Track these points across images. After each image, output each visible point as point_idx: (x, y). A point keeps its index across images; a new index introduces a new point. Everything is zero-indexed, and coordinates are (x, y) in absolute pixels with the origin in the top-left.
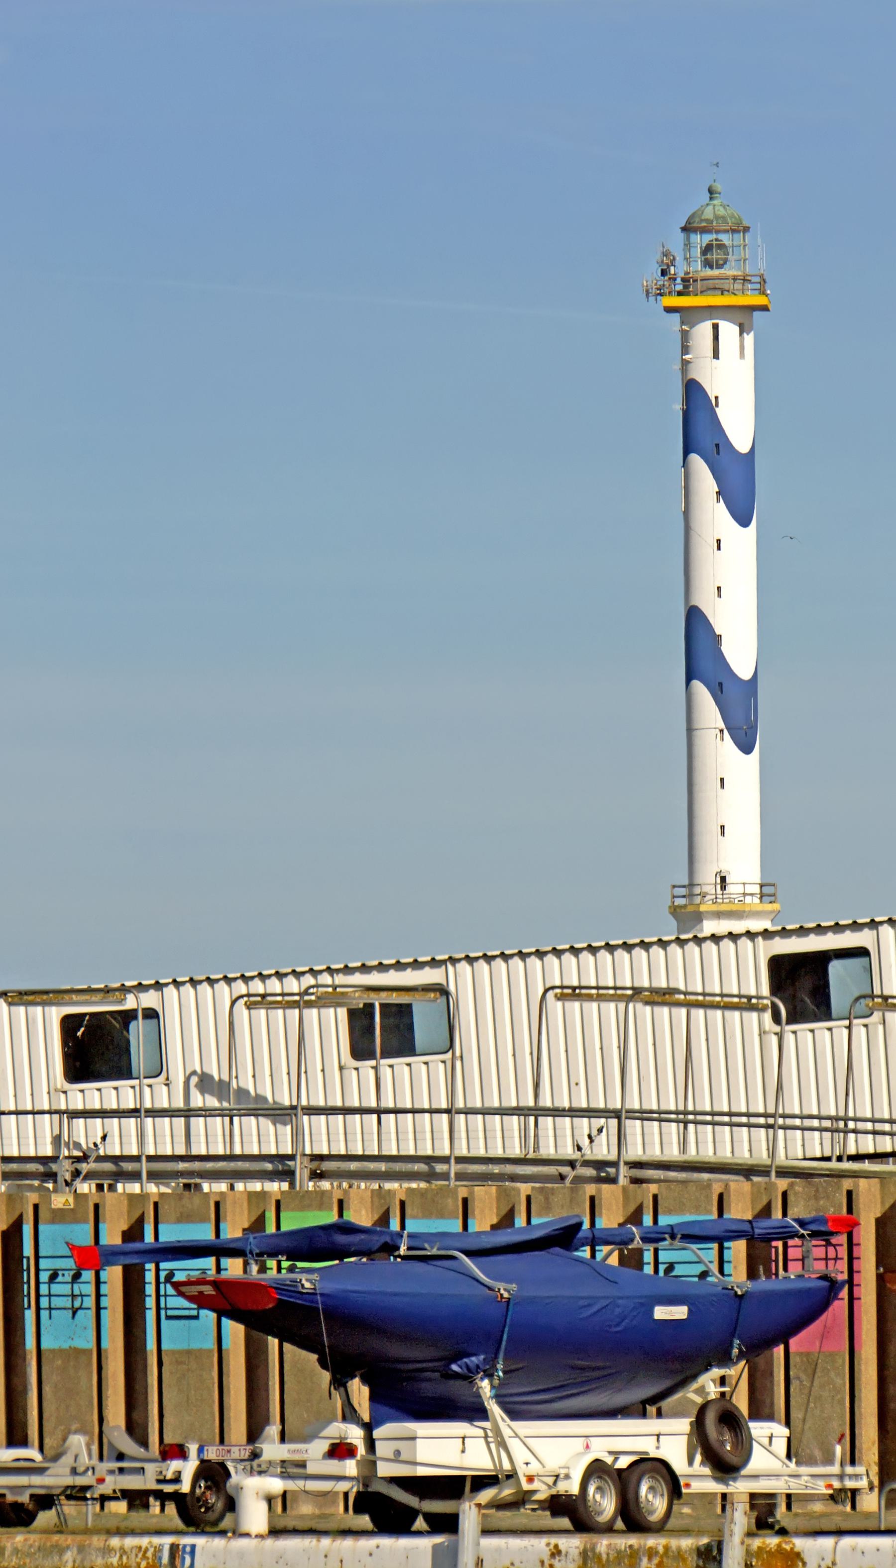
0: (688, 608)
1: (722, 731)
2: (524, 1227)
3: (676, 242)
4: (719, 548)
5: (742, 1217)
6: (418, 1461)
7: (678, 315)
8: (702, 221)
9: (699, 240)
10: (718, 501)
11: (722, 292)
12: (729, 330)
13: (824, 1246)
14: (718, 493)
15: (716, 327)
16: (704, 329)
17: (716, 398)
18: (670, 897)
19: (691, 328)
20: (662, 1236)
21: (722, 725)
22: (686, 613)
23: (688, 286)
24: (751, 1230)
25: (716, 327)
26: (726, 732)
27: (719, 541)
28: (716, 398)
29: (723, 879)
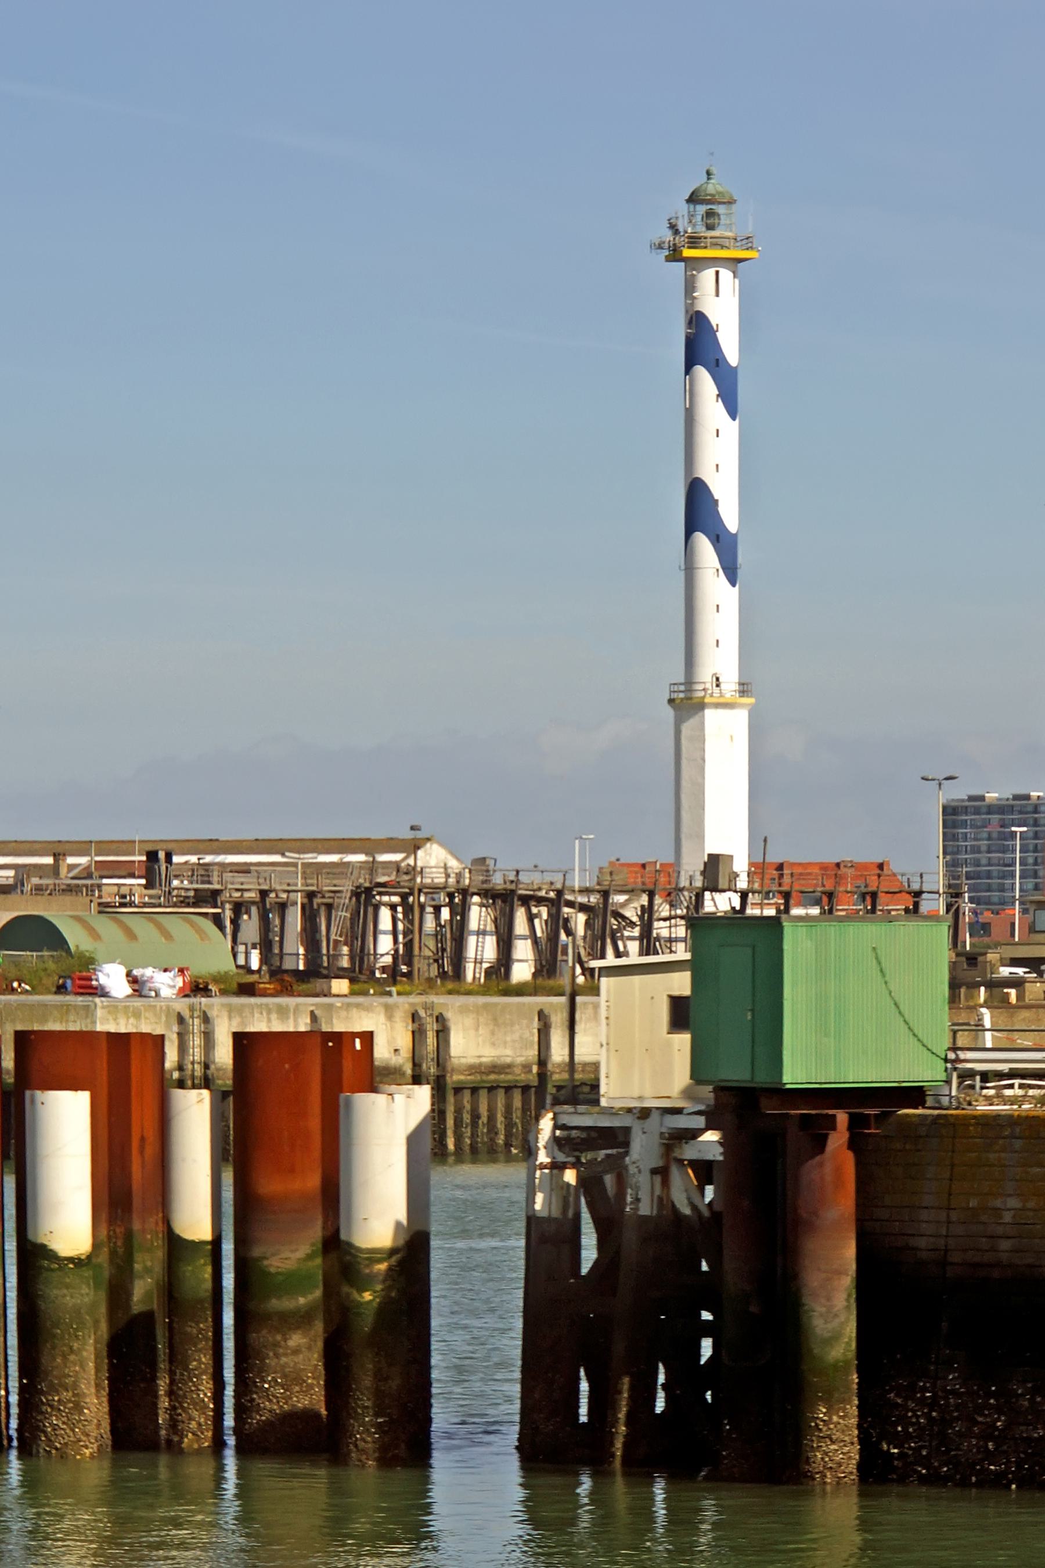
0: (690, 480)
1: (718, 570)
2: (441, 844)
3: (683, 208)
4: (718, 611)
5: (13, 1274)
6: (567, 1059)
7: (683, 264)
8: (707, 195)
9: (702, 209)
10: (717, 401)
11: (722, 247)
12: (726, 274)
13: (520, 889)
14: (718, 396)
15: (717, 273)
16: (708, 275)
17: (717, 325)
18: (668, 692)
19: (699, 272)
20: (576, 954)
21: (718, 566)
22: (687, 487)
23: (694, 242)
24: (1012, 1212)
25: (717, 273)
26: (721, 571)
27: (718, 641)
28: (717, 325)
29: (718, 679)
